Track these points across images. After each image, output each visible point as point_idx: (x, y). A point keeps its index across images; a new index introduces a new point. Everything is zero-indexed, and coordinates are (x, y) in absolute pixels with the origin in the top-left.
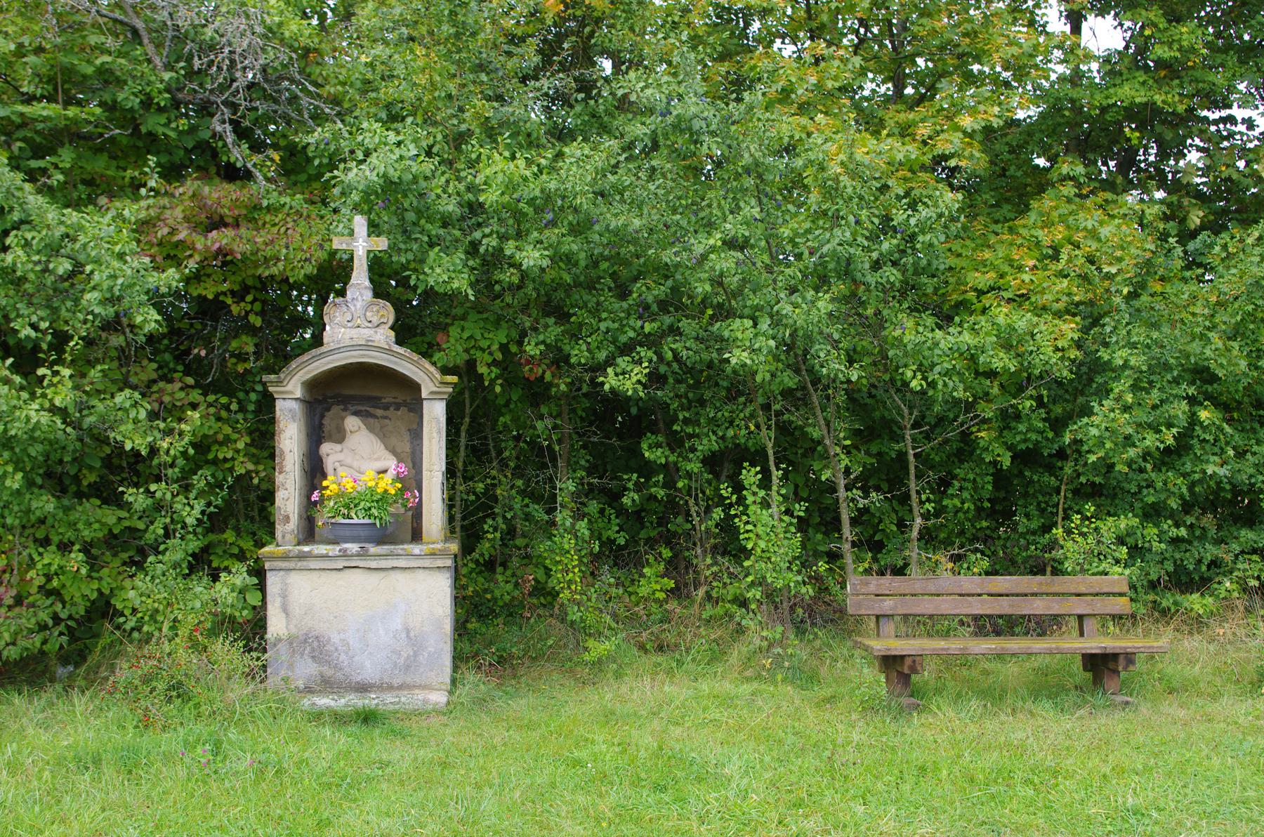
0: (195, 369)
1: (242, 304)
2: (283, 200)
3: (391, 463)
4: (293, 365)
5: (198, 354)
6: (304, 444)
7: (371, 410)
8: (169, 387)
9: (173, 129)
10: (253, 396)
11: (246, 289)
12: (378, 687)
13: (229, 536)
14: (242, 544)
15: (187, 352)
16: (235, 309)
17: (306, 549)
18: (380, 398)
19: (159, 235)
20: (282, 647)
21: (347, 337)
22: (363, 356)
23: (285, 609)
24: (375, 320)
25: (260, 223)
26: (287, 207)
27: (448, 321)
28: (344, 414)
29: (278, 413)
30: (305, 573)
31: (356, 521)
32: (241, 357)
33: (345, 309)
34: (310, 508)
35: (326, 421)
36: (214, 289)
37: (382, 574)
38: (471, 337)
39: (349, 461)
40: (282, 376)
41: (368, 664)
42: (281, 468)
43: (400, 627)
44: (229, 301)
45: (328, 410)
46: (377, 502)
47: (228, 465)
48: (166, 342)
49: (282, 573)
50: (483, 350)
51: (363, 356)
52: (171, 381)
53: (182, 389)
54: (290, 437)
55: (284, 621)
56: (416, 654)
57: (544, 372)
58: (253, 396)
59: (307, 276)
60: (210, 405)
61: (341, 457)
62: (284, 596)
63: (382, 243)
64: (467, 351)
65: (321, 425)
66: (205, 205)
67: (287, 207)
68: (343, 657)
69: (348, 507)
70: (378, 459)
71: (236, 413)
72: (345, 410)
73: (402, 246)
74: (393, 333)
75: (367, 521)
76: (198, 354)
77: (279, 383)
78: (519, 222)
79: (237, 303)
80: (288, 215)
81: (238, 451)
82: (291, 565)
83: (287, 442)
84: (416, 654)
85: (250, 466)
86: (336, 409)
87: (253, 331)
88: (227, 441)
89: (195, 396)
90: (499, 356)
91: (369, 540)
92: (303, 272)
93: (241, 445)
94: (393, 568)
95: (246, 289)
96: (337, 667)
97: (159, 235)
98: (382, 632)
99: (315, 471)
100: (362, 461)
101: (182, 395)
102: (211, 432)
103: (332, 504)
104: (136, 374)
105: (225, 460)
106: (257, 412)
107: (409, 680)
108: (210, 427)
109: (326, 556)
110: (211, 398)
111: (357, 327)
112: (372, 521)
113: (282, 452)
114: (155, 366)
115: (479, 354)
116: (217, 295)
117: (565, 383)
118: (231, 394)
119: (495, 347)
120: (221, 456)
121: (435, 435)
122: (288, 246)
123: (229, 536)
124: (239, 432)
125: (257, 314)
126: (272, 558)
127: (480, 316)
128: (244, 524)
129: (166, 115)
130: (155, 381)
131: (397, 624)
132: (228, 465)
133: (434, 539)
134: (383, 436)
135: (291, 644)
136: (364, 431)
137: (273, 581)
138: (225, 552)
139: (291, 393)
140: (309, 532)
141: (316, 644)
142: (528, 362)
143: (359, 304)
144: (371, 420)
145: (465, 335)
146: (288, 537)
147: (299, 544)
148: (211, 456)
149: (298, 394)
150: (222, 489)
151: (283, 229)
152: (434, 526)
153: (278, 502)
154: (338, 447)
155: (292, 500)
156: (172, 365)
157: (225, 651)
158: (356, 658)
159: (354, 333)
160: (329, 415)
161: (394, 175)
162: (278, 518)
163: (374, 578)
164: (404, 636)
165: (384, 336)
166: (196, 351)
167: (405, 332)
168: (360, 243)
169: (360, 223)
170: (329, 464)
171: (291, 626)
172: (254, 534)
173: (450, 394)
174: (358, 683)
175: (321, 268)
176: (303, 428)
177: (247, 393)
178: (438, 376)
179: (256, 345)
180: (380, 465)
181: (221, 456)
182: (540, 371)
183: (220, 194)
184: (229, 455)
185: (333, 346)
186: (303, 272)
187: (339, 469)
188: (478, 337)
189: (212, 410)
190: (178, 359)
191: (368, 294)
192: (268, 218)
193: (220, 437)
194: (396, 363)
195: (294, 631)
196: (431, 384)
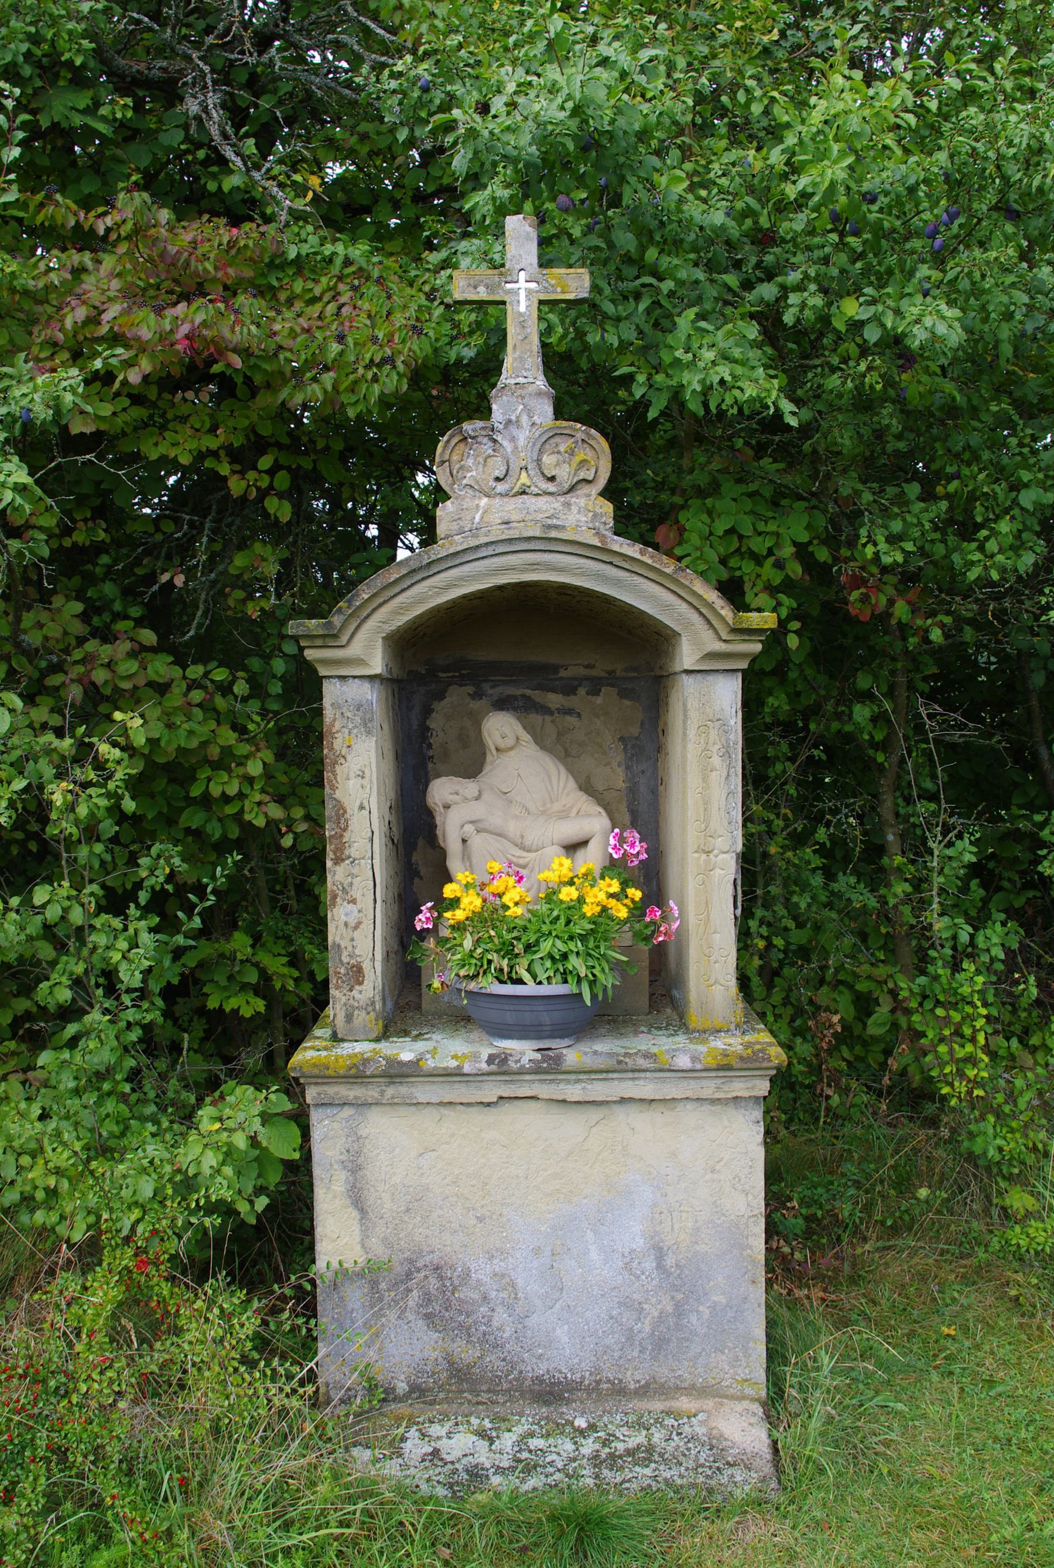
0: (163, 613)
1: (251, 475)
2: (328, 249)
3: (594, 822)
4: (364, 593)
5: (170, 583)
6: (390, 782)
7: (536, 695)
8: (106, 651)
9: (103, 119)
10: (279, 666)
11: (258, 445)
12: (589, 1391)
13: (240, 942)
14: (265, 959)
15: (151, 578)
16: (236, 486)
17: (405, 1051)
18: (556, 668)
19: (69, 323)
20: (355, 1296)
21: (495, 518)
22: (534, 566)
23: (357, 1199)
24: (565, 474)
25: (283, 296)
26: (338, 261)
27: (677, 500)
28: (475, 705)
29: (329, 713)
30: (403, 1111)
31: (530, 989)
32: (250, 586)
33: (487, 448)
34: (405, 941)
35: (435, 723)
36: (192, 445)
37: (594, 1115)
38: (731, 531)
39: (496, 820)
40: (337, 620)
41: (562, 1333)
42: (340, 849)
43: (639, 1243)
44: (224, 469)
45: (440, 696)
46: (583, 938)
47: (230, 810)
48: (105, 559)
49: (347, 1112)
50: (758, 559)
51: (534, 566)
52: (107, 637)
53: (132, 654)
54: (360, 774)
55: (356, 1228)
56: (679, 1311)
57: (891, 602)
58: (279, 666)
59: (384, 402)
60: (193, 685)
61: (477, 810)
62: (354, 1167)
63: (575, 283)
64: (723, 561)
65: (425, 730)
66: (163, 255)
67: (338, 261)
68: (501, 1317)
69: (507, 950)
70: (563, 815)
71: (245, 700)
72: (478, 695)
73: (609, 308)
74: (608, 508)
75: (557, 989)
76: (170, 583)
77: (329, 639)
78: (872, 240)
79: (242, 473)
80: (340, 278)
81: (250, 780)
82: (371, 1093)
83: (353, 784)
84: (679, 1311)
85: (276, 812)
86: (457, 696)
87: (276, 531)
88: (225, 761)
89: (161, 667)
90: (795, 569)
91: (561, 1031)
92: (376, 388)
93: (254, 768)
94: (623, 1101)
95: (258, 445)
96: (489, 1342)
97: (69, 323)
98: (594, 1255)
99: (418, 854)
100: (526, 828)
101: (132, 666)
102: (194, 744)
103: (468, 943)
104: (40, 626)
105: (226, 799)
106: (286, 698)
107: (663, 1373)
108: (191, 733)
109: (454, 1075)
110: (195, 671)
111: (517, 497)
112: (570, 988)
113: (341, 811)
114: (78, 607)
115: (748, 567)
116: (201, 456)
117: (942, 625)
118: (234, 662)
119: (787, 551)
120: (215, 791)
121: (716, 761)
122: (348, 332)
123: (240, 942)
124: (250, 741)
125: (281, 496)
126: (324, 1076)
127: (742, 488)
128: (270, 921)
129: (90, 93)
130: (81, 641)
131: (632, 1235)
132: (230, 810)
133: (718, 1023)
134: (562, 749)
135: (374, 1284)
136: (529, 748)
137: (329, 1135)
138: (231, 978)
139: (359, 662)
140: (408, 999)
141: (433, 1283)
142: (858, 582)
143: (523, 436)
144: (536, 718)
145: (721, 526)
146: (361, 1018)
147: (384, 1035)
148: (196, 792)
149: (377, 665)
150: (203, 897)
151: (331, 308)
152: (717, 991)
153: (334, 934)
154: (470, 787)
155: (367, 926)
156: (117, 607)
157: (215, 1323)
158: (533, 1321)
159: (512, 508)
160: (441, 708)
161: (602, 119)
162: (336, 970)
163: (572, 1126)
164: (649, 1264)
165: (588, 515)
166: (165, 578)
167: (641, 511)
168: (521, 278)
169: (520, 233)
170: (452, 828)
171: (374, 1242)
172: (289, 941)
173: (754, 659)
174: (539, 1380)
175: (417, 376)
176: (388, 746)
177: (267, 658)
178: (726, 612)
179: (285, 563)
180: (571, 830)
181: (215, 791)
182: (883, 600)
183: (204, 240)
184: (232, 790)
185: (460, 543)
186: (376, 388)
187: (477, 842)
188: (747, 530)
189: (197, 696)
190: (129, 593)
191: (545, 410)
192: (298, 286)
193: (214, 752)
194: (617, 583)
195: (379, 1251)
196: (707, 635)
